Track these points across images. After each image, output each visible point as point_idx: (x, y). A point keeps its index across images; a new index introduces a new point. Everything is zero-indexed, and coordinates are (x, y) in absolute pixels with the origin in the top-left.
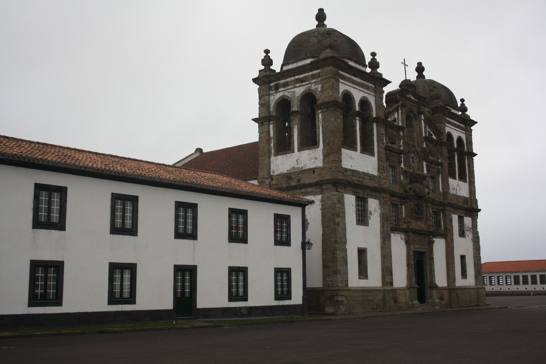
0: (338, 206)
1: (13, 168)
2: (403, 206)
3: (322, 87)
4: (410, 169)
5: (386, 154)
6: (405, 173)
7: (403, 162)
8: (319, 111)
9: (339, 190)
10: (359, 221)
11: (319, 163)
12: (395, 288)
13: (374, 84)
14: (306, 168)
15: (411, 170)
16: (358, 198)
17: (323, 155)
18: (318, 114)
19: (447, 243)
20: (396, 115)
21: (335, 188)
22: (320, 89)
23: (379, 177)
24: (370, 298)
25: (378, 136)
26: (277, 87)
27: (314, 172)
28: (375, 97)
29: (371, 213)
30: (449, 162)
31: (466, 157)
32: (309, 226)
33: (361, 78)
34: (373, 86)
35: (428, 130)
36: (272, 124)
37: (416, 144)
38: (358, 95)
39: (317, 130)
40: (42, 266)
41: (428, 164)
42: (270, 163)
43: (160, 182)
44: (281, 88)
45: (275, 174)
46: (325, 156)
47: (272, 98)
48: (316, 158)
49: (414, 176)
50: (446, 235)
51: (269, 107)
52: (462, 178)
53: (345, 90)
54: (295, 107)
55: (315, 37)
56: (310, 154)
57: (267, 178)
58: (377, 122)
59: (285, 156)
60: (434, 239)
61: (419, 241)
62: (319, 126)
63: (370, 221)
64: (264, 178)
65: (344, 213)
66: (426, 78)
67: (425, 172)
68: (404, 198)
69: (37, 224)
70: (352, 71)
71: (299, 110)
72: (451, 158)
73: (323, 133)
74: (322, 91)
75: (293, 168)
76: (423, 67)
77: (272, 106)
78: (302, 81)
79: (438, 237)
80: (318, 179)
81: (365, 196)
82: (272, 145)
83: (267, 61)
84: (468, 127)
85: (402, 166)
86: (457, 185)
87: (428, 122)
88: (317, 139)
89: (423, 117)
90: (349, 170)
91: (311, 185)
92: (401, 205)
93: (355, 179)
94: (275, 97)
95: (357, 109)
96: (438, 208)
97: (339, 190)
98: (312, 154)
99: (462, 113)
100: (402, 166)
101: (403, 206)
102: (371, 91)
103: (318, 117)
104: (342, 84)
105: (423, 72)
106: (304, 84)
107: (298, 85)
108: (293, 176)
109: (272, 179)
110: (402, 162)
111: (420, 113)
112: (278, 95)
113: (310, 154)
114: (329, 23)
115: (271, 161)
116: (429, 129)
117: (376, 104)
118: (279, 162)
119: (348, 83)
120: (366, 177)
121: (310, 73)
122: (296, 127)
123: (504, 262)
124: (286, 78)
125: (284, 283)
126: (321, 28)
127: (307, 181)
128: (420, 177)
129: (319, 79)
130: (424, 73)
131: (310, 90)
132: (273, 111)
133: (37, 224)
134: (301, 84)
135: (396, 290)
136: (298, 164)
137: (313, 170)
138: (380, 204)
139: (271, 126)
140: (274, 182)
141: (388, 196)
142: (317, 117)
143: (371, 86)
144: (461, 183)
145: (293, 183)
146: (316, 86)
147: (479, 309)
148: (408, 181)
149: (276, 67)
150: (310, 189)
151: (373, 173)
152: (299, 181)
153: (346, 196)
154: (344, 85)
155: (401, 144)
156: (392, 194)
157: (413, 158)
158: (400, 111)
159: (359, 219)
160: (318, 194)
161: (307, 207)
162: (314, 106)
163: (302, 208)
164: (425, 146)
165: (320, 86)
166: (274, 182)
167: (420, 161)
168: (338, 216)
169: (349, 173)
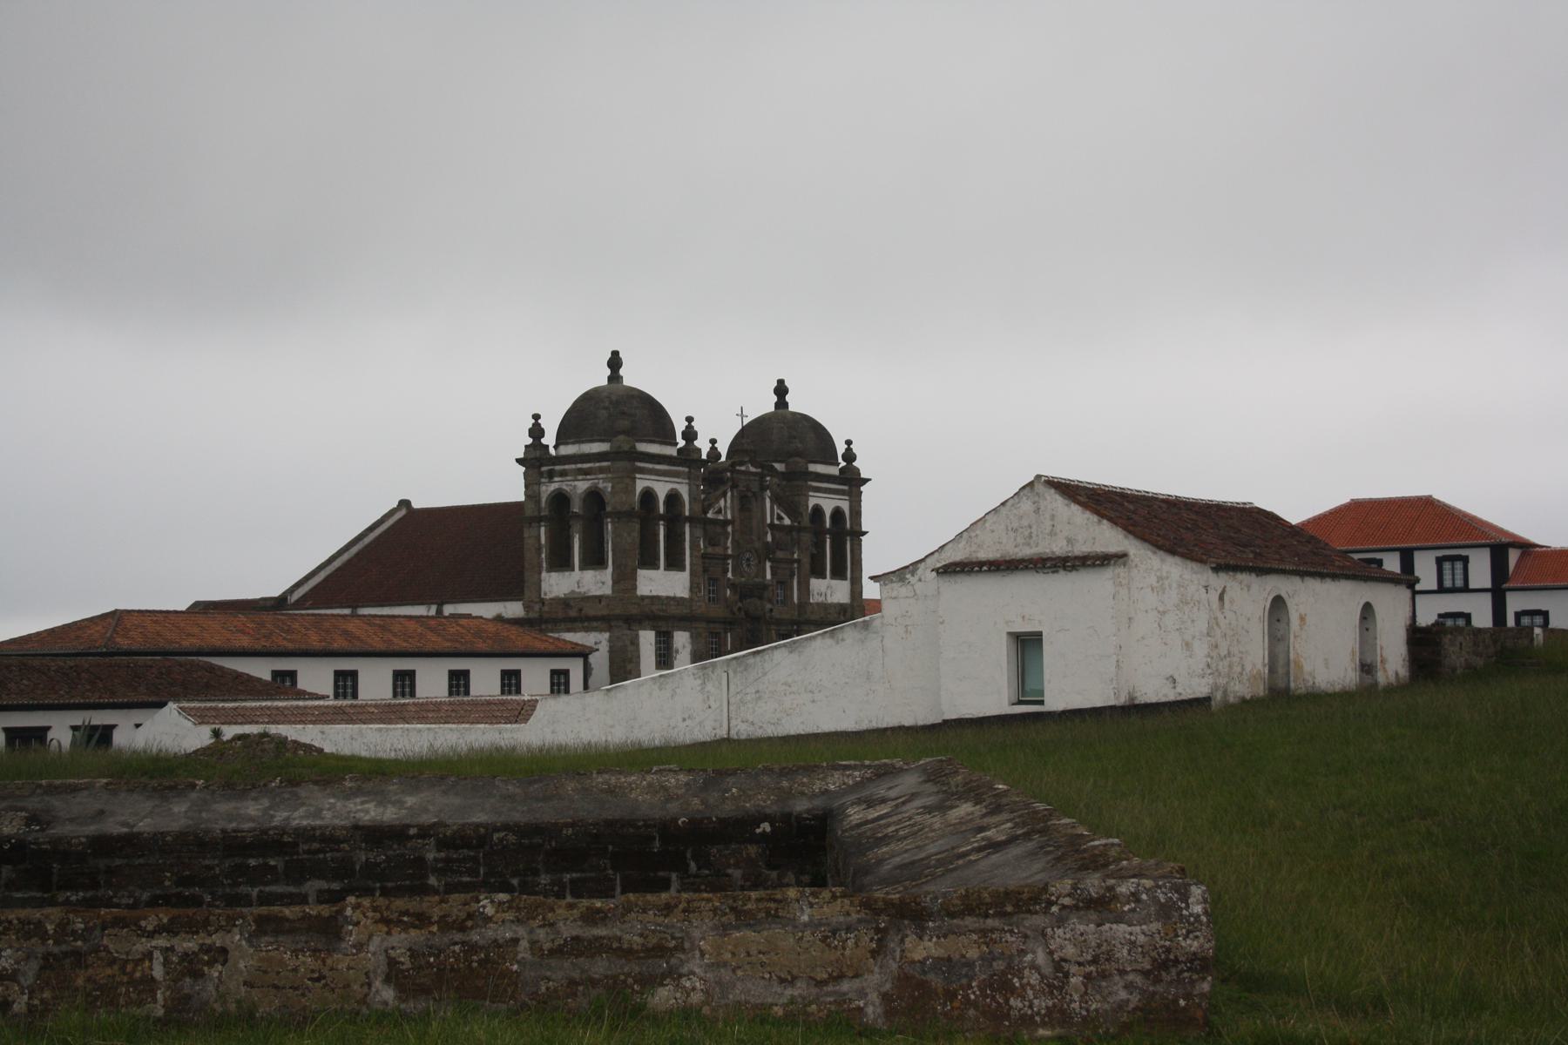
0: (631, 648)
1: (320, 659)
2: (729, 634)
3: (613, 487)
4: (743, 577)
5: (704, 563)
6: (733, 586)
7: (730, 570)
8: (609, 520)
9: (634, 628)
11: (607, 590)
13: (688, 467)
14: (591, 594)
15: (743, 579)
16: (658, 634)
17: (613, 580)
18: (607, 525)
20: (722, 503)
22: (609, 489)
23: (691, 599)
25: (691, 541)
26: (551, 475)
27: (600, 602)
28: (689, 485)
29: (677, 652)
30: (815, 552)
31: (848, 538)
32: (594, 672)
34: (686, 470)
35: (776, 510)
37: (754, 538)
38: (662, 489)
39: (605, 546)
42: (540, 580)
44: (557, 477)
45: (547, 597)
46: (615, 582)
47: (543, 488)
48: (603, 583)
51: (539, 502)
52: (838, 573)
53: (644, 488)
54: (576, 508)
55: (606, 408)
56: (595, 576)
57: (536, 603)
58: (690, 522)
59: (561, 574)
62: (608, 540)
64: (532, 601)
65: (639, 657)
66: (792, 408)
67: (769, 576)
68: (730, 623)
72: (820, 546)
73: (613, 550)
74: (613, 492)
75: (573, 592)
76: (786, 387)
77: (544, 500)
78: (586, 472)
80: (605, 612)
81: (670, 629)
82: (543, 556)
83: (537, 432)
84: (854, 489)
85: (730, 575)
86: (828, 587)
87: (776, 500)
88: (606, 557)
89: (768, 493)
90: (648, 597)
91: (596, 618)
92: (726, 633)
93: (654, 608)
94: (548, 489)
95: (662, 510)
96: (790, 628)
97: (634, 628)
98: (599, 577)
100: (730, 575)
101: (729, 634)
102: (684, 479)
103: (607, 528)
106: (588, 477)
107: (580, 477)
108: (572, 603)
109: (543, 603)
110: (728, 571)
111: (763, 489)
112: (553, 487)
113: (595, 576)
114: (795, 404)
115: (542, 578)
116: (778, 508)
117: (690, 495)
118: (553, 581)
119: (648, 477)
120: (672, 602)
121: (597, 464)
122: (577, 536)
124: (565, 464)
126: (614, 386)
127: (591, 613)
128: (325, 1010)
129: (610, 475)
130: (788, 398)
131: (597, 487)
132: (545, 508)
134: (584, 477)
136: (579, 587)
137: (599, 598)
138: (691, 637)
139: (543, 530)
140: (546, 608)
141: (704, 625)
142: (605, 527)
143: (684, 471)
144: (836, 583)
145: (573, 613)
146: (605, 484)
148: (737, 597)
149: (549, 439)
150: (595, 624)
151: (682, 595)
152: (581, 610)
153: (642, 633)
155: (729, 544)
156: (709, 621)
157: (748, 560)
158: (729, 494)
159: (660, 662)
160: (605, 631)
161: (590, 656)
162: (602, 512)
164: (769, 538)
165: (610, 485)
166: (546, 608)
167: (760, 562)
168: (631, 661)
169: (646, 601)
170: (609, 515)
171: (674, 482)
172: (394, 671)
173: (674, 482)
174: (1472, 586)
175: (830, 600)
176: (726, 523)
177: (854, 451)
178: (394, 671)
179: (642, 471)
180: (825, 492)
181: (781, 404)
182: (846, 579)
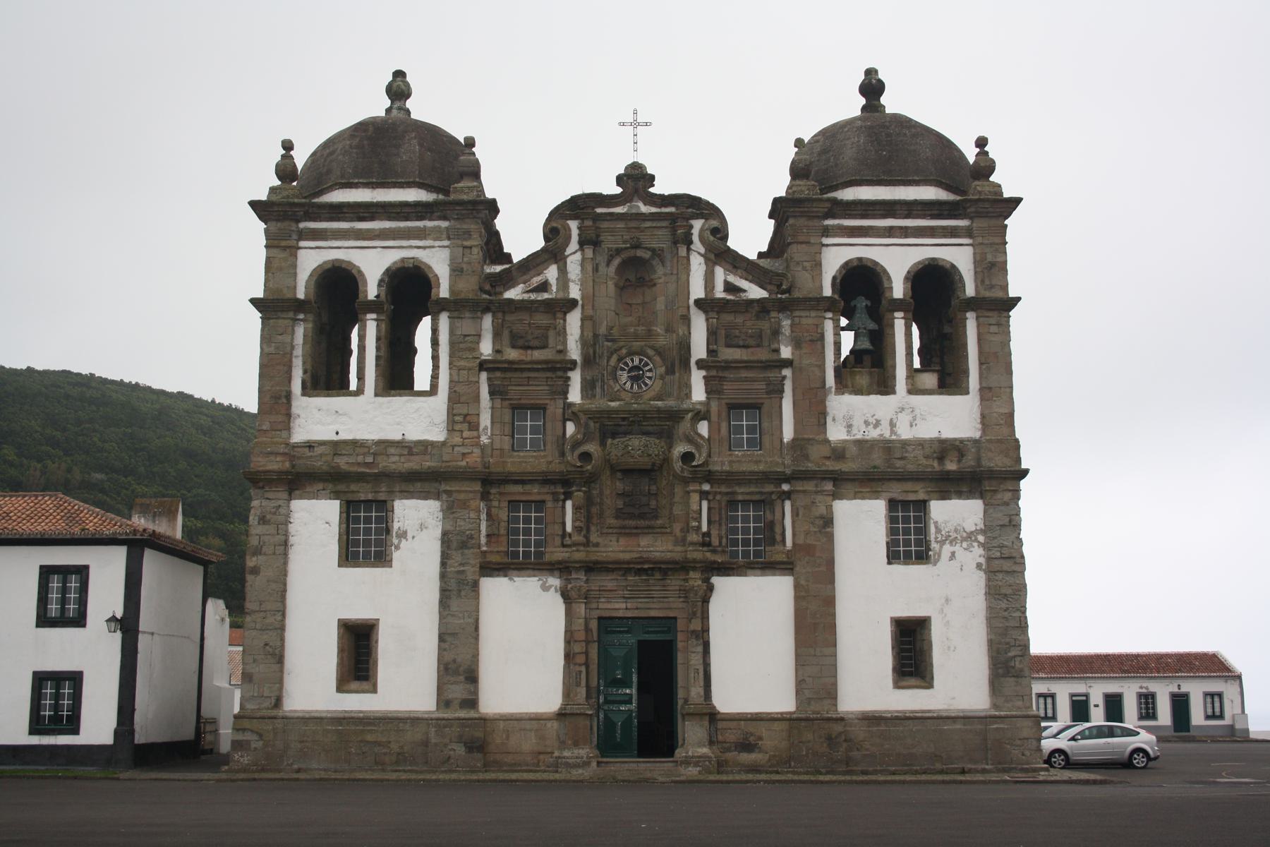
12: (484, 713)
16: (350, 509)
19: (801, 596)
24: (369, 738)
33: (390, 219)
40: (51, 679)
43: (29, 539)
49: (624, 419)
50: (792, 563)
61: (629, 590)
63: (396, 555)
69: (44, 620)
70: (345, 213)
79: (749, 571)
104: (317, 250)
105: (881, 98)
114: (420, 109)
123: (477, 638)
133: (44, 620)
135: (485, 720)
154: (322, 250)
163: (128, 547)
170: (299, 306)
171: (411, 247)
172: (42, 567)
173: (411, 247)
174: (461, 401)
175: (905, 433)
178: (42, 567)
179: (827, 232)
180: (933, 236)
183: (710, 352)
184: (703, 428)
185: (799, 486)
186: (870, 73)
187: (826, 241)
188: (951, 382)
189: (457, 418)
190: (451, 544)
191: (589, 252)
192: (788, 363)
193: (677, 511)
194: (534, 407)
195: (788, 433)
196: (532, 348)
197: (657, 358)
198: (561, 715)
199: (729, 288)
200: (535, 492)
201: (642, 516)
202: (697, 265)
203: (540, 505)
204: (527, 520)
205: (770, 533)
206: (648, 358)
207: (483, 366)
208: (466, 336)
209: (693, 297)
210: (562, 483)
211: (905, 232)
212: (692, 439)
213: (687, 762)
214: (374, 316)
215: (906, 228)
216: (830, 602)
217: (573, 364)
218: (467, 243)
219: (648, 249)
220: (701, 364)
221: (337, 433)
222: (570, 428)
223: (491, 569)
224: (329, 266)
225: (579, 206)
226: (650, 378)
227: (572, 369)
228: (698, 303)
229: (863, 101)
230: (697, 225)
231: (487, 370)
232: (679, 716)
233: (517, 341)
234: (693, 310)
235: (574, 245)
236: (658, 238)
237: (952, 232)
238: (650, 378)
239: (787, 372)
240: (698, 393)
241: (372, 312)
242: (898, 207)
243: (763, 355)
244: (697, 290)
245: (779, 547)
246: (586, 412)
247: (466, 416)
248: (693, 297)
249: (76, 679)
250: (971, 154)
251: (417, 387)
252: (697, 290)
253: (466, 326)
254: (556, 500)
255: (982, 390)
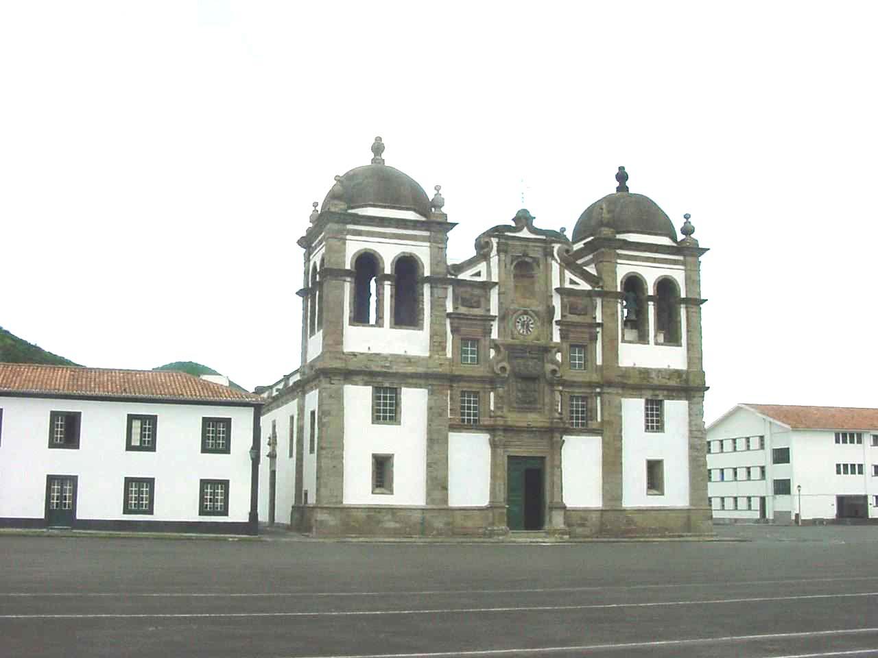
9: (333, 382)
10: (391, 418)
19: (605, 445)
21: (328, 379)
36: (348, 282)
41: (564, 328)
50: (603, 430)
60: (564, 438)
66: (631, 191)
71: (353, 270)
99: (597, 366)
114: (391, 159)
125: (132, 487)
130: (628, 183)
147: (648, 542)
170: (348, 273)
176: (487, 286)
177: (692, 224)
180: (391, 238)
181: (623, 188)
182: (681, 346)
183: (563, 316)
184: (559, 357)
185: (606, 390)
186: (379, 139)
187: (619, 261)
188: (672, 338)
189: (436, 344)
190: (434, 413)
191: (502, 256)
192: (599, 325)
193: (547, 400)
194: (472, 340)
195: (599, 362)
196: (472, 307)
197: (536, 318)
198: (491, 507)
199: (572, 282)
200: (476, 387)
201: (530, 402)
202: (556, 267)
203: (476, 394)
204: (469, 402)
205: (589, 414)
206: (532, 317)
207: (449, 315)
208: (440, 298)
209: (554, 287)
210: (492, 381)
211: (655, 260)
212: (554, 362)
213: (549, 533)
214: (389, 283)
215: (655, 258)
216: (620, 450)
217: (493, 318)
218: (440, 246)
219: (531, 257)
220: (558, 323)
221: (369, 348)
222: (492, 353)
223: (454, 428)
224: (363, 251)
225: (498, 231)
226: (532, 328)
227: (493, 320)
228: (557, 290)
229: (617, 184)
230: (556, 247)
231: (450, 318)
232: (547, 510)
233: (466, 302)
234: (554, 293)
235: (494, 252)
236: (536, 253)
237: (675, 262)
238: (532, 328)
239: (599, 329)
240: (556, 338)
241: (388, 280)
242: (392, 222)
243: (588, 320)
244: (556, 284)
245: (594, 422)
246: (503, 345)
247: (440, 342)
248: (554, 287)
249: (225, 484)
250: (431, 196)
251: (371, 323)
252: (556, 284)
253: (439, 292)
254: (485, 392)
255: (688, 344)
